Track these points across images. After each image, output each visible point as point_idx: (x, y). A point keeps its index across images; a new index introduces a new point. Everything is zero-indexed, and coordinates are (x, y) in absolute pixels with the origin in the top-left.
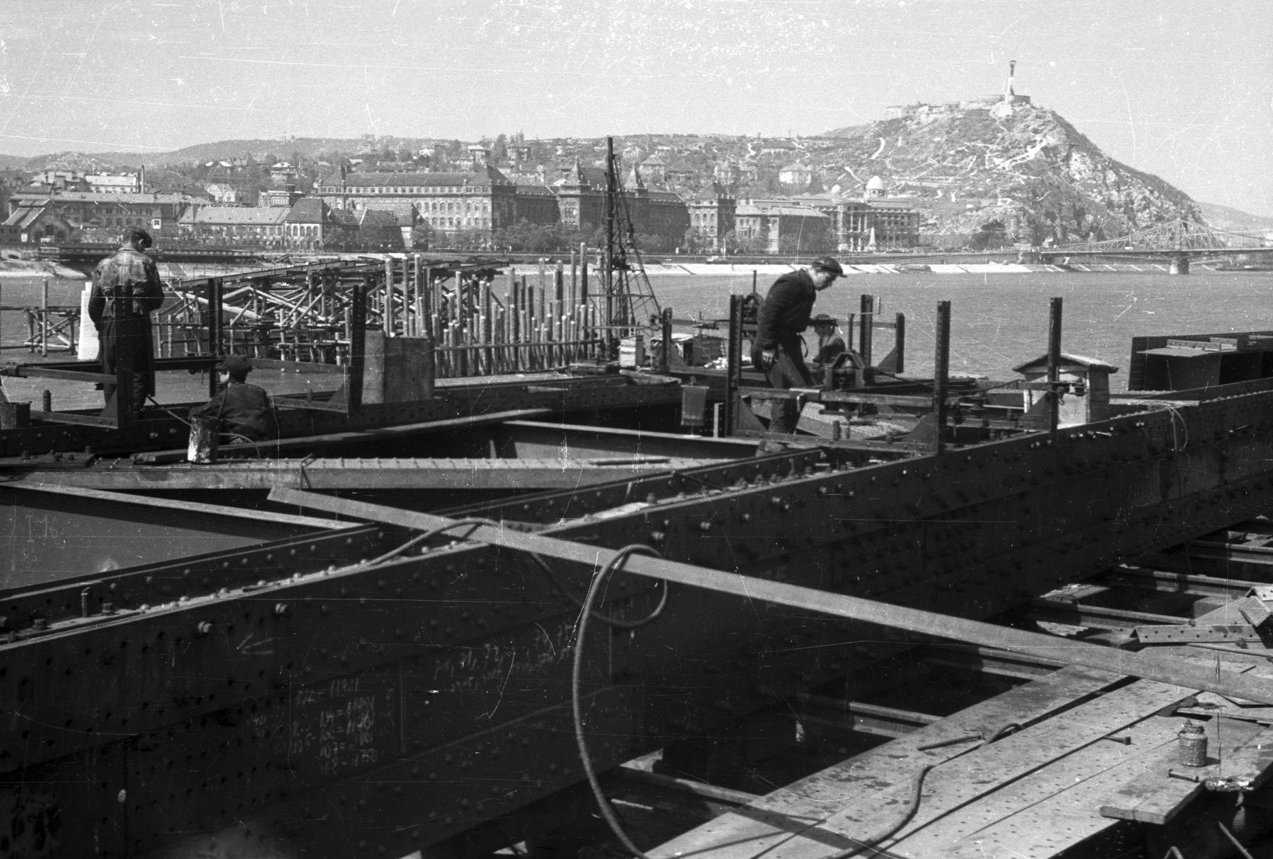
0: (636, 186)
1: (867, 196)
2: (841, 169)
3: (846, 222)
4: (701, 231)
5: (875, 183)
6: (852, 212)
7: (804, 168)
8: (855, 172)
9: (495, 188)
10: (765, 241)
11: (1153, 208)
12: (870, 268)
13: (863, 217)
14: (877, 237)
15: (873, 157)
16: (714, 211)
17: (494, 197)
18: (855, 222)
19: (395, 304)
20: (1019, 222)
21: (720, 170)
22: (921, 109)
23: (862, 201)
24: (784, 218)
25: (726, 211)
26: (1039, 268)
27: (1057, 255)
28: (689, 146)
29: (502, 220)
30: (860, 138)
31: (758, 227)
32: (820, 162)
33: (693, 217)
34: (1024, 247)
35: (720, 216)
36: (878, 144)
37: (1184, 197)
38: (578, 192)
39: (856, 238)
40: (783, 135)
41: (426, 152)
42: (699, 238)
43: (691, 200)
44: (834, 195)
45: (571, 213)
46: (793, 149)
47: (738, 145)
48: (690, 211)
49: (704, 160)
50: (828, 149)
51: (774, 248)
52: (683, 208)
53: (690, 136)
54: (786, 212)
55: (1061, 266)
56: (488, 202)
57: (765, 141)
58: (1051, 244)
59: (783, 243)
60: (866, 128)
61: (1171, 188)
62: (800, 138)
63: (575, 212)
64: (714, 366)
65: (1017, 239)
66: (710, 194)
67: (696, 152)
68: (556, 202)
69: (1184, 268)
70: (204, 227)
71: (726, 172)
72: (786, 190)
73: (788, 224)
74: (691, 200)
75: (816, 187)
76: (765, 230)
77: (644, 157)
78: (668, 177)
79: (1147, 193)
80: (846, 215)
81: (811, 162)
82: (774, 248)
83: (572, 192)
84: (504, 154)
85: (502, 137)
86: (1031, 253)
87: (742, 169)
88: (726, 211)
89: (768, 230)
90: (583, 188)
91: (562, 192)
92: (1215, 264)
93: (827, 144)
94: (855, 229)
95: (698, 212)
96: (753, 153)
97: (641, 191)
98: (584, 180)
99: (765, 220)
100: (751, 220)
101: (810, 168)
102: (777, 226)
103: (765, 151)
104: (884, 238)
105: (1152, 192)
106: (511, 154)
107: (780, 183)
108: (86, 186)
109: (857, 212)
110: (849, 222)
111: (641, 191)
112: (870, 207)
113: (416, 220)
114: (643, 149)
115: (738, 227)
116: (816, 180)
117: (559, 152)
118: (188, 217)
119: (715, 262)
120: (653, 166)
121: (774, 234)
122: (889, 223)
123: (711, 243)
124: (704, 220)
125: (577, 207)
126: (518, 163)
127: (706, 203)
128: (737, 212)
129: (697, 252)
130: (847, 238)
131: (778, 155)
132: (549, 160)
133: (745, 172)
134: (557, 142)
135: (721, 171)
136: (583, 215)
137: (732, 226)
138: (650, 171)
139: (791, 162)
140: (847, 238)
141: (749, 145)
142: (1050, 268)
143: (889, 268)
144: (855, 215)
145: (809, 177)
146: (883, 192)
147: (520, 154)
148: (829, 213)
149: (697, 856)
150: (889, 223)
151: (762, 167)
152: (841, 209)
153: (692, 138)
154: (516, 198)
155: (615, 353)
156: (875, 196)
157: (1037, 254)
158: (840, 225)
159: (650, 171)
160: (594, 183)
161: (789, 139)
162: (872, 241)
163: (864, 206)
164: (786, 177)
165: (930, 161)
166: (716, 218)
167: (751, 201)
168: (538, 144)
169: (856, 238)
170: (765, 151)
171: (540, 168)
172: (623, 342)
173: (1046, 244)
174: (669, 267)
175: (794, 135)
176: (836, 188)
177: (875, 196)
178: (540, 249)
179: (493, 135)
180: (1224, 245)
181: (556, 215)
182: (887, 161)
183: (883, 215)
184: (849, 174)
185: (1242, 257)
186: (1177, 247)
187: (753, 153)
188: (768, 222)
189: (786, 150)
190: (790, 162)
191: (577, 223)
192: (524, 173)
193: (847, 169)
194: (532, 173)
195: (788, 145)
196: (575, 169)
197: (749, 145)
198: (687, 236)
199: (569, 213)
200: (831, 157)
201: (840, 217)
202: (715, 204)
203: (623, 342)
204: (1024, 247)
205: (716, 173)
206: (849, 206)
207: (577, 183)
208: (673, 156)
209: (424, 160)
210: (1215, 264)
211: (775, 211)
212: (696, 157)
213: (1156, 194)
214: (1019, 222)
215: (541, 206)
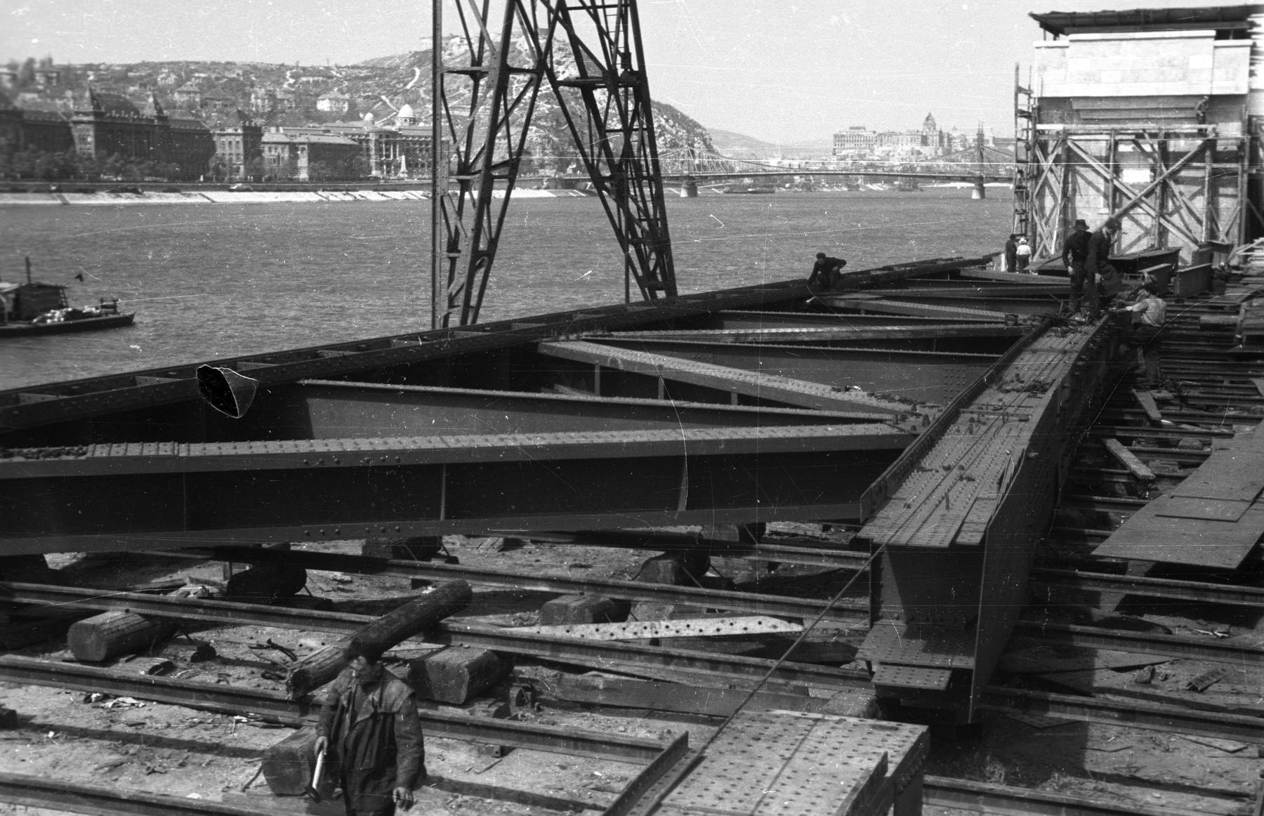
0: (155, 113)
1: (398, 124)
2: (378, 98)
3: (379, 150)
4: (227, 157)
5: (406, 111)
6: (384, 140)
7: (341, 97)
8: (391, 100)
10: (296, 170)
11: (668, 136)
12: (398, 195)
13: (395, 144)
14: (408, 165)
15: (408, 87)
16: (239, 139)
18: (387, 150)
19: (541, 180)
20: (544, 149)
21: (257, 98)
22: (453, 41)
23: (394, 129)
24: (312, 146)
25: (253, 136)
26: (563, 193)
27: (578, 180)
28: (227, 74)
30: (398, 67)
31: (286, 155)
32: (357, 91)
33: (218, 144)
34: (549, 172)
35: (245, 143)
36: (413, 74)
37: (697, 125)
38: (91, 118)
39: (389, 165)
40: (321, 63)
42: (224, 165)
43: (215, 127)
44: (367, 123)
45: (86, 140)
46: (332, 77)
47: (275, 73)
48: (215, 139)
49: (243, 85)
50: (366, 78)
53: (228, 63)
54: (314, 139)
55: (583, 191)
57: (304, 69)
58: (574, 170)
59: (312, 170)
61: (683, 116)
62: (338, 67)
63: (89, 139)
64: (44, 320)
65: (542, 166)
66: (233, 120)
67: (232, 80)
68: (69, 128)
69: (692, 191)
71: (263, 100)
72: (321, 118)
73: (318, 152)
74: (215, 127)
75: (353, 115)
76: (294, 158)
77: (180, 82)
78: (204, 104)
79: (663, 122)
80: (378, 142)
81: (349, 90)
82: (303, 175)
83: (86, 119)
84: (32, 78)
85: (31, 62)
86: (554, 179)
87: (279, 96)
88: (253, 136)
89: (297, 157)
90: (96, 114)
91: (75, 118)
92: (722, 187)
93: (364, 73)
94: (388, 156)
95: (223, 139)
96: (292, 81)
97: (161, 117)
98: (97, 106)
99: (293, 147)
100: (280, 147)
101: (347, 96)
102: (306, 153)
103: (304, 79)
104: (416, 165)
105: (667, 121)
106: (40, 78)
107: (316, 110)
109: (389, 139)
110: (381, 150)
111: (161, 117)
112: (401, 135)
114: (179, 76)
115: (266, 154)
116: (353, 105)
117: (91, 78)
119: (238, 190)
120: (188, 93)
121: (303, 162)
122: (421, 150)
123: (238, 170)
124: (229, 145)
125: (92, 133)
126: (46, 88)
127: (230, 131)
128: (264, 139)
129: (221, 181)
131: (316, 83)
132: (80, 86)
133: (282, 100)
134: (90, 67)
135: (258, 100)
136: (99, 142)
137: (260, 152)
138: (185, 98)
140: (380, 165)
141: (288, 74)
142: (573, 193)
144: (387, 143)
145: (346, 105)
146: (414, 121)
147: (49, 79)
148: (361, 141)
149: (162, 811)
150: (421, 150)
151: (300, 95)
153: (229, 65)
156: (406, 124)
157: (560, 179)
158: (373, 152)
159: (185, 98)
160: (109, 109)
161: (328, 68)
162: (403, 168)
163: (395, 134)
165: (462, 91)
166: (241, 145)
167: (281, 129)
168: (68, 69)
169: (389, 165)
170: (304, 79)
171: (69, 93)
173: (569, 170)
174: (189, 196)
175: (332, 64)
176: (369, 116)
177: (406, 124)
178: (49, 177)
179: (21, 59)
180: (732, 169)
181: (70, 141)
182: (421, 91)
183: (414, 143)
184: (385, 103)
185: (747, 181)
186: (686, 172)
187: (292, 81)
188: (297, 149)
189: (324, 79)
190: (328, 90)
191: (92, 151)
192: (53, 98)
193: (384, 97)
194: (61, 98)
195: (326, 73)
196: (87, 94)
197: (288, 74)
198: (212, 165)
199: (83, 140)
200: (368, 86)
201: (372, 146)
202: (240, 131)
204: (549, 172)
205: (253, 101)
206: (381, 134)
207: (90, 109)
208: (209, 84)
210: (722, 187)
211: (303, 139)
212: (228, 85)
213: (671, 122)
214: (544, 149)
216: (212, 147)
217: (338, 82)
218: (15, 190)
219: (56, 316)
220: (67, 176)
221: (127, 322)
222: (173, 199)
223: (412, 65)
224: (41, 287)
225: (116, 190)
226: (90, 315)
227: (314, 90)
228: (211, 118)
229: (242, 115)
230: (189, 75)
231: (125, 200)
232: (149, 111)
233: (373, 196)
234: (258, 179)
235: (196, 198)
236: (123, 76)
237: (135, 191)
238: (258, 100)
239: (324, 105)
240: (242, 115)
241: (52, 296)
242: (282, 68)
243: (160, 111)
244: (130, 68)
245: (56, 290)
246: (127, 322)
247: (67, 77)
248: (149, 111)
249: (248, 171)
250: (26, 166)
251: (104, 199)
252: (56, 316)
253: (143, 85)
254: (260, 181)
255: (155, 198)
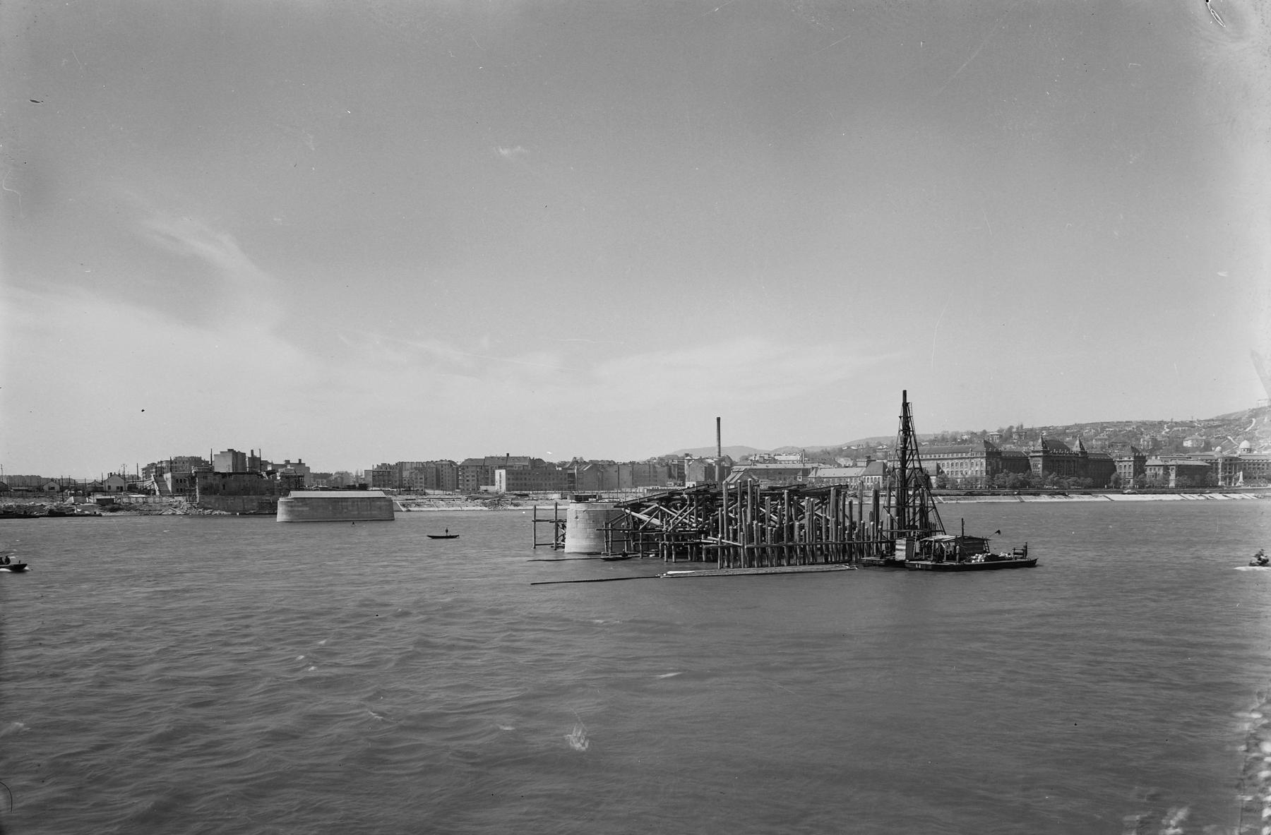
2: (1225, 438)
3: (1224, 469)
9: (988, 453)
10: (1168, 481)
14: (1245, 478)
17: (987, 458)
24: (1179, 466)
25: (1140, 463)
29: (992, 472)
31: (1161, 472)
40: (1187, 419)
41: (965, 437)
44: (1217, 453)
45: (1038, 466)
51: (1172, 484)
52: (1111, 462)
54: (1180, 462)
56: (984, 461)
60: (1243, 413)
70: (820, 479)
72: (1186, 450)
73: (1181, 470)
75: (1208, 447)
76: (1167, 473)
78: (1111, 446)
80: (1223, 464)
82: (1172, 484)
85: (1011, 427)
88: (1140, 463)
93: (1217, 423)
97: (1083, 451)
98: (1045, 447)
99: (1166, 468)
108: (775, 461)
113: (939, 471)
115: (1148, 472)
118: (812, 474)
121: (1173, 476)
124: (1125, 468)
129: (1118, 487)
130: (1224, 479)
134: (1044, 428)
137: (1144, 471)
139: (1191, 435)
140: (1224, 479)
143: (1251, 495)
146: (1250, 450)
152: (1220, 461)
153: (1128, 423)
154: (1002, 458)
155: (892, 548)
164: (1188, 444)
172: (898, 541)
176: (1219, 448)
178: (1013, 487)
179: (1006, 427)
181: (1028, 467)
199: (1036, 466)
203: (898, 541)
207: (1041, 448)
208: (1115, 434)
209: (964, 441)
211: (1173, 463)
212: (1126, 435)
215: (1020, 463)
216: (1114, 469)
217: (1199, 429)
218: (993, 494)
219: (979, 558)
220: (1025, 487)
221: (1032, 564)
222: (1086, 498)
223: (1251, 417)
224: (970, 538)
225: (1052, 494)
226: (1003, 558)
227: (1182, 435)
228: (1114, 454)
229: (1134, 449)
230: (1103, 429)
231: (1057, 499)
232: (1076, 448)
233: (1219, 497)
234: (1142, 487)
235: (1101, 498)
236: (1064, 431)
237: (1063, 494)
238: (1144, 442)
239: (1188, 444)
240: (1134, 449)
241: (978, 544)
242: (1161, 423)
243: (1082, 448)
244: (1068, 428)
245: (982, 541)
246: (1032, 564)
247: (1030, 434)
248: (1076, 448)
249: (1136, 482)
250: (1001, 481)
251: (1044, 499)
252: (979, 558)
253: (1075, 437)
254: (1142, 488)
255: (1076, 498)
